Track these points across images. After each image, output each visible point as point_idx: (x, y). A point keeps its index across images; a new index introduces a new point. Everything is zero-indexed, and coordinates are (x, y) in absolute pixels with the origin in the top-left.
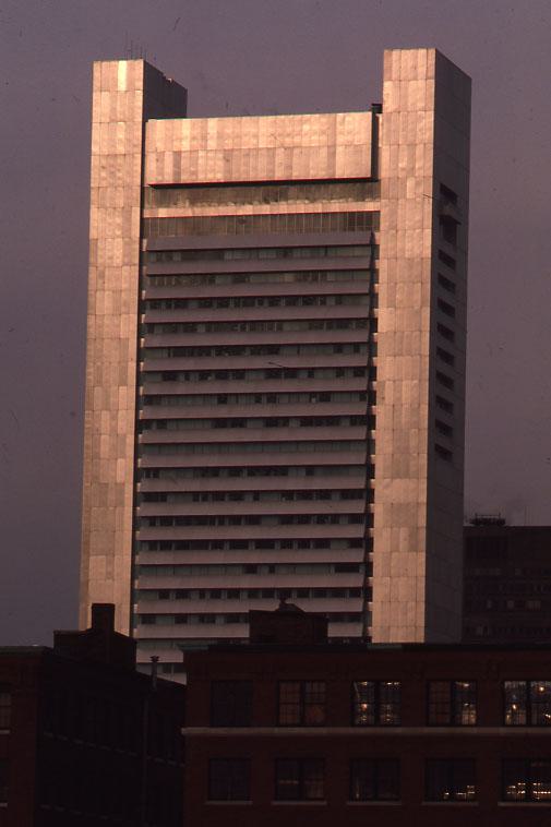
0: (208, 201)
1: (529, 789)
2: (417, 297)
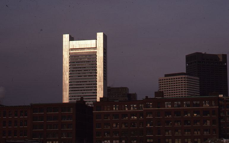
0: (84, 50)
1: (134, 117)
2: (102, 61)
